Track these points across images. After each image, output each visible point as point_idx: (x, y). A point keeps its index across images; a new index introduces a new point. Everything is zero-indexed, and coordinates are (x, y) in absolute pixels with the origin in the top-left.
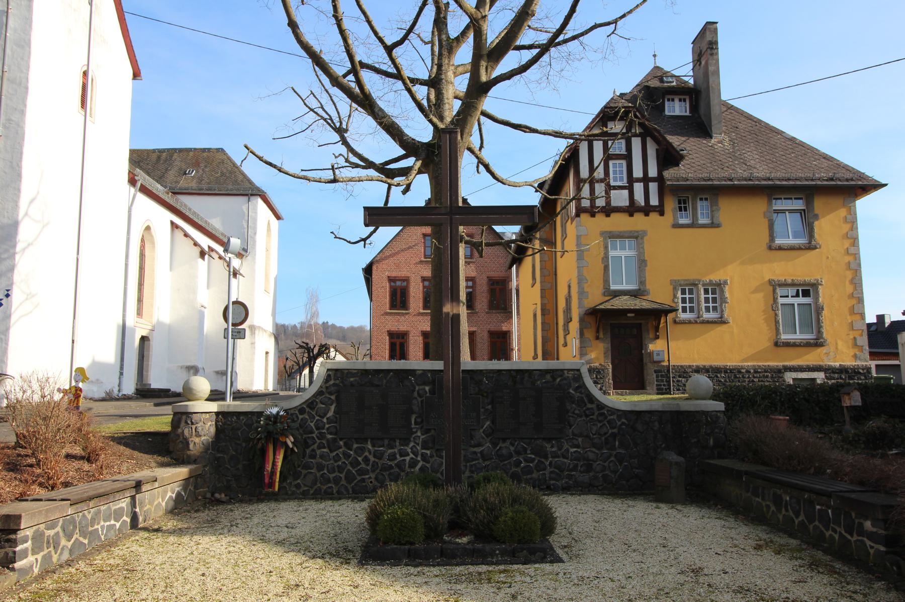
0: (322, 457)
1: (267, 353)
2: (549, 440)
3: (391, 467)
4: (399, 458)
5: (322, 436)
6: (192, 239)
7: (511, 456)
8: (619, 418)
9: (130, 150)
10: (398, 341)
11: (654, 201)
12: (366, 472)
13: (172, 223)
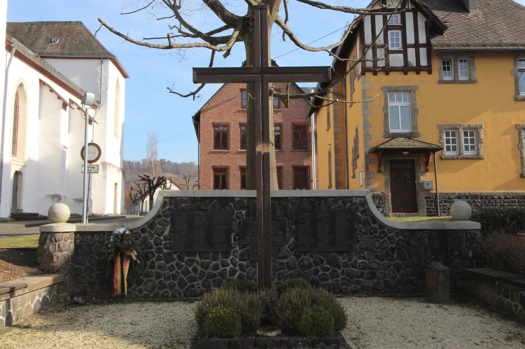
0: (159, 267)
2: (341, 253)
3: (215, 275)
4: (221, 268)
5: (159, 251)
6: (57, 94)
7: (310, 266)
12: (195, 279)
13: (41, 81)
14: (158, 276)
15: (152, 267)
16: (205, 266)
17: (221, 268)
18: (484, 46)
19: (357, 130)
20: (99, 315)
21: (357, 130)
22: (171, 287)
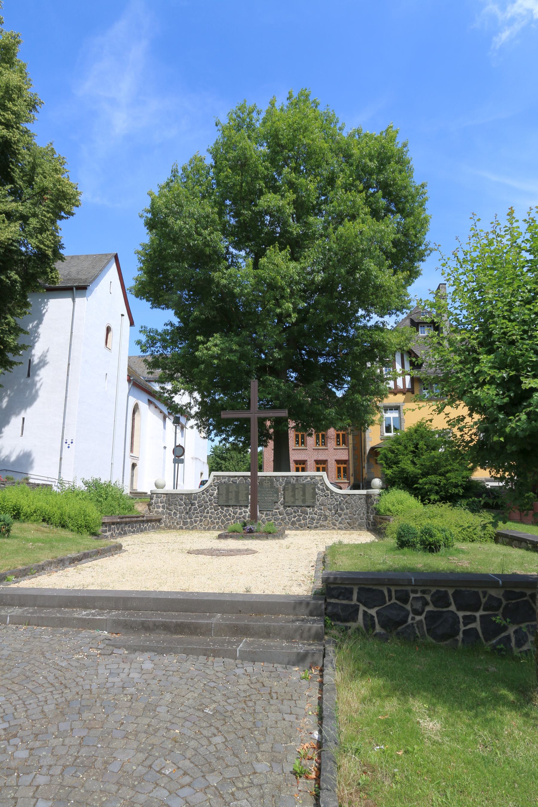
0: (211, 513)
1: (108, 330)
2: (309, 507)
3: (240, 518)
4: (244, 514)
5: (211, 504)
6: (159, 409)
7: (292, 514)
8: (340, 497)
9: (129, 358)
10: (342, 466)
11: (408, 385)
12: (230, 520)
13: (149, 400)
14: (211, 517)
15: (208, 513)
16: (235, 513)
17: (244, 514)
18: (323, 534)
19: (199, 552)
20: (491, 272)
21: (199, 552)
22: (218, 523)
